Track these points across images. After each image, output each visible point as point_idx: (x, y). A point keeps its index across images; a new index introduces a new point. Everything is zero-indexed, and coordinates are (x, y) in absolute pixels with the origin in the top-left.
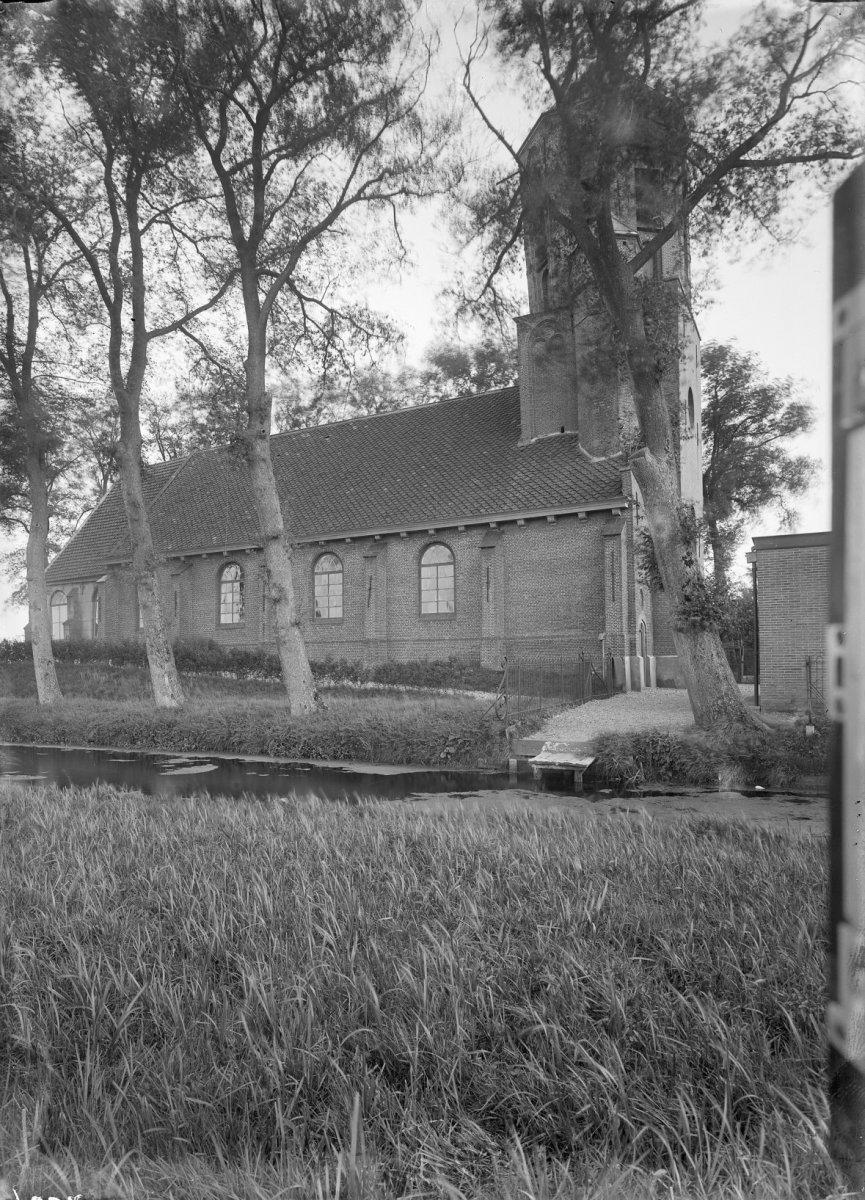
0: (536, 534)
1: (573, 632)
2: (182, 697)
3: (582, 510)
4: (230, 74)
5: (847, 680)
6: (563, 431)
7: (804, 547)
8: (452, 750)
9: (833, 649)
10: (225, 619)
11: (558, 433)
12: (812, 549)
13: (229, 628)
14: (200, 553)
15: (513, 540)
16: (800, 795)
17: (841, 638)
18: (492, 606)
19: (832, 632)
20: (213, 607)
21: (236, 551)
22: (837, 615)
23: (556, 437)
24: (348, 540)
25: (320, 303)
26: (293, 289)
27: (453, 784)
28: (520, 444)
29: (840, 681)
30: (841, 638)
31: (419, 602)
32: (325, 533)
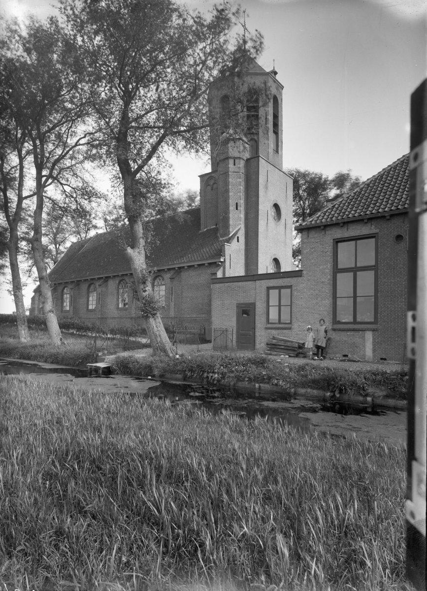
0: (192, 273)
1: (204, 316)
2: (29, 338)
3: (206, 262)
4: (111, 67)
5: (417, 339)
6: (216, 225)
7: (231, 282)
8: (80, 361)
9: (410, 323)
10: (90, 307)
11: (214, 227)
12: (229, 284)
13: (92, 311)
14: (204, 262)
15: (185, 275)
16: (4, 360)
17: (414, 318)
18: (173, 304)
19: (410, 314)
20: (86, 302)
21: (161, 270)
22: (412, 305)
23: (214, 228)
24: (186, 267)
25: (69, 186)
26: (58, 181)
27: (80, 374)
28: (200, 232)
29: (413, 340)
30: (414, 318)
31: (88, 305)
32: (198, 261)
